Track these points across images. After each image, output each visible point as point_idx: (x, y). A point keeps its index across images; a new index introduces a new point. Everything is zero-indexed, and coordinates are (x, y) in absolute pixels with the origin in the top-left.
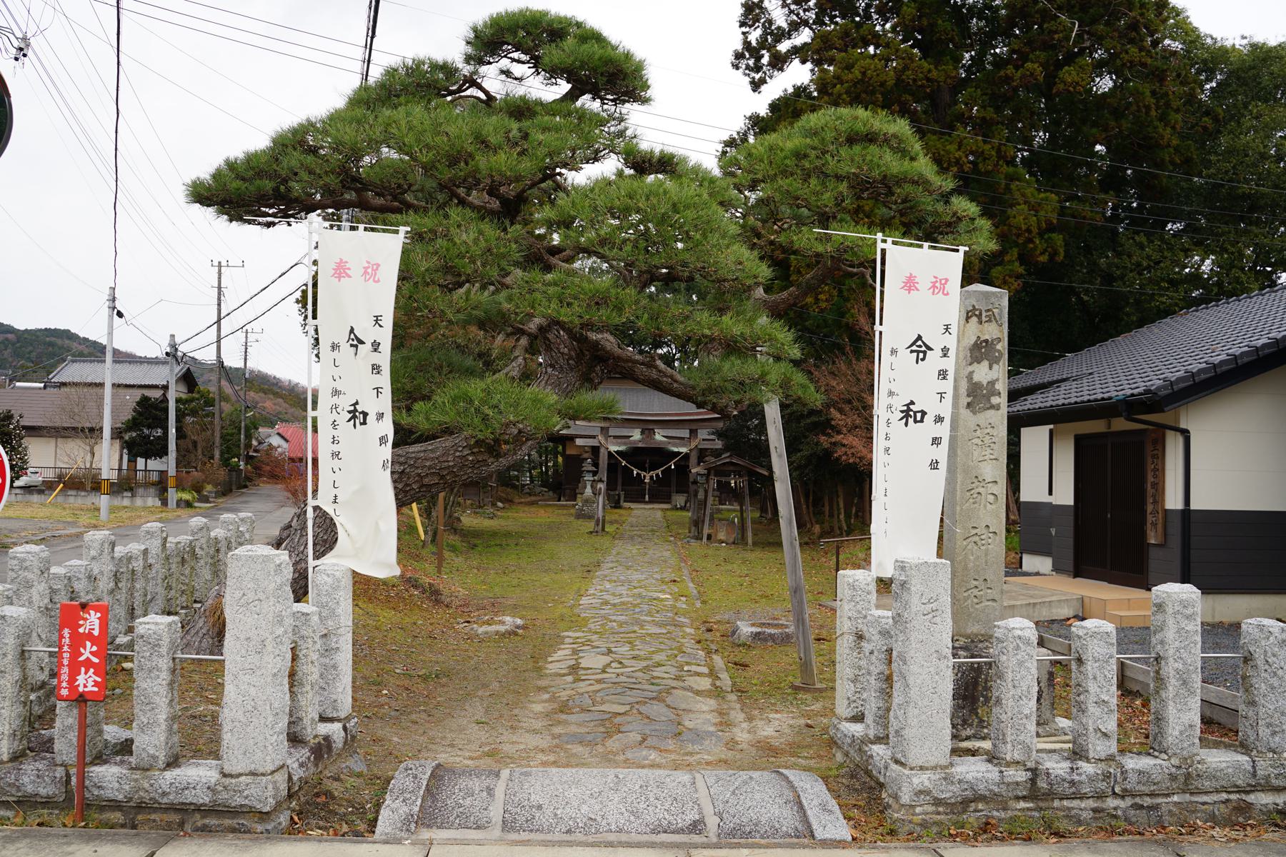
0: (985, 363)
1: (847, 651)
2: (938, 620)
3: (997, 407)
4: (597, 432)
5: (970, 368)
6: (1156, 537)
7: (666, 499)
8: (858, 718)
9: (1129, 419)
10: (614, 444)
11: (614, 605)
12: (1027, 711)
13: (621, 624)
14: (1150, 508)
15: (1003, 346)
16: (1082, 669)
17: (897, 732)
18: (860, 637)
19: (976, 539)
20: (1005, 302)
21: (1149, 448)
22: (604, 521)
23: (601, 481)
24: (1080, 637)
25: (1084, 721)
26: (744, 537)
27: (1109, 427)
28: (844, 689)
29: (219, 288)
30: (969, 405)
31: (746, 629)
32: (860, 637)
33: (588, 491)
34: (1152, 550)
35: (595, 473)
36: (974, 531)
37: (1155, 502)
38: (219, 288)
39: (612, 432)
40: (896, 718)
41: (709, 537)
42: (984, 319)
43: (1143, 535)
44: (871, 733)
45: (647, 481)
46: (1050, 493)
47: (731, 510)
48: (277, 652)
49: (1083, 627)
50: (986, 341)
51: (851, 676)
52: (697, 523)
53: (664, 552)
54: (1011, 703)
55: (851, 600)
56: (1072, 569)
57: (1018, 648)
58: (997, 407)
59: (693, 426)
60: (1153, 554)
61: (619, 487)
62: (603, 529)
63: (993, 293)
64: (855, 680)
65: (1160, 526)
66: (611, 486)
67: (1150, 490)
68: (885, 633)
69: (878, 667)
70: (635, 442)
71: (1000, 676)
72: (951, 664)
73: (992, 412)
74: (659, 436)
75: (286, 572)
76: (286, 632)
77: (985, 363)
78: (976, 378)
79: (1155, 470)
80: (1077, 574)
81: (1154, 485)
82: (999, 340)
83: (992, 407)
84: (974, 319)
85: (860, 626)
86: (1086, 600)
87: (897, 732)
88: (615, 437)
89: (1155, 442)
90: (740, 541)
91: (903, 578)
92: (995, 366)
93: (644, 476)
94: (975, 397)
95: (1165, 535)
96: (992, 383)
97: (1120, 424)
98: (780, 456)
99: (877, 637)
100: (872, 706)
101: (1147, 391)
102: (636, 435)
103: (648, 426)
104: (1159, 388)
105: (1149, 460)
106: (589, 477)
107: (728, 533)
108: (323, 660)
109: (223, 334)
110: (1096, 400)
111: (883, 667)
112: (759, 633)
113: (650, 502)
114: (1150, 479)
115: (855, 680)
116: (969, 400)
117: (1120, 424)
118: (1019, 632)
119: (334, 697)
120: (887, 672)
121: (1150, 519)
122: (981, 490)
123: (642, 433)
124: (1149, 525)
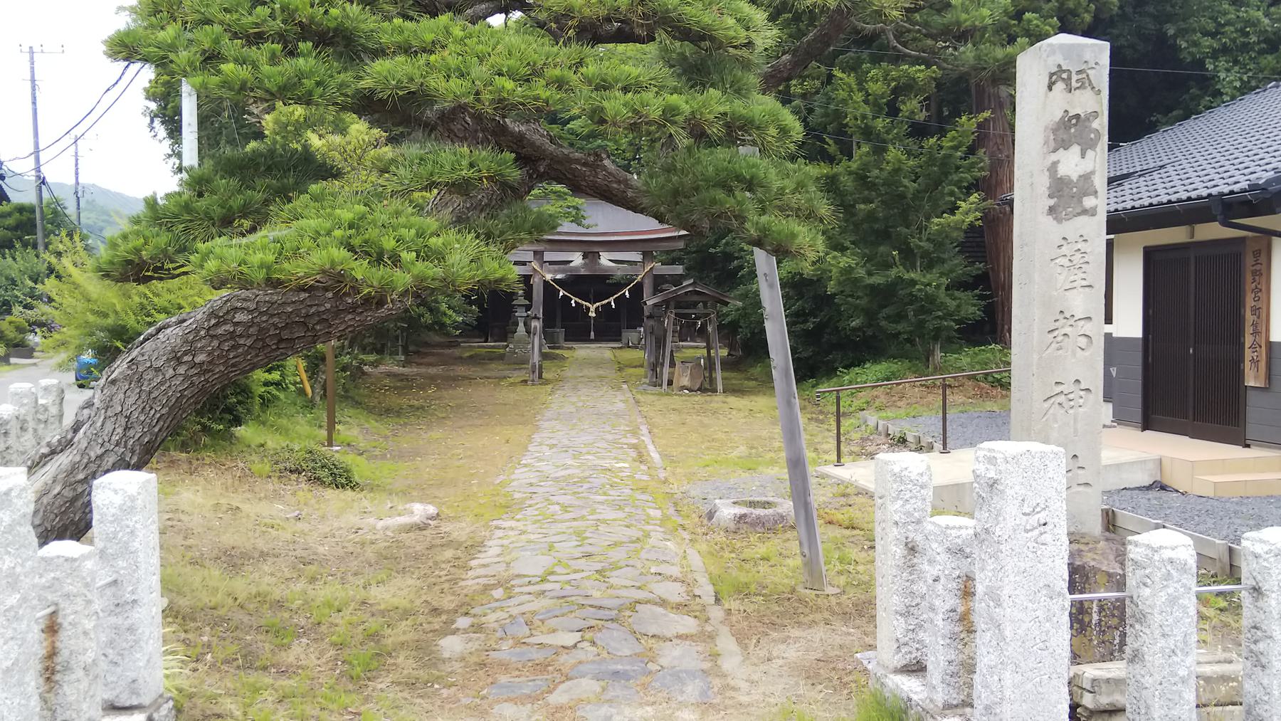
0: (1076, 149)
1: (894, 572)
2: (1047, 538)
3: (1092, 212)
4: (529, 256)
5: (1054, 157)
6: (1256, 378)
7: (616, 337)
8: (916, 668)
9: (1226, 224)
10: (550, 272)
11: (556, 479)
12: (1183, 672)
13: (565, 508)
14: (1248, 340)
15: (1102, 124)
16: (1260, 604)
17: (987, 708)
18: (912, 549)
19: (1061, 399)
20: (1105, 60)
21: (1249, 260)
22: (540, 367)
23: (536, 318)
24: (1257, 557)
25: (1265, 682)
26: (712, 380)
27: (1192, 236)
28: (889, 627)
29: (33, 80)
30: (1051, 210)
31: (727, 512)
32: (912, 549)
33: (521, 328)
34: (1250, 393)
35: (528, 308)
36: (1059, 389)
37: (1256, 333)
38: (33, 80)
39: (549, 256)
40: (986, 686)
41: (670, 383)
42: (1074, 84)
43: (1239, 374)
44: (940, 698)
45: (592, 314)
46: (1109, 320)
47: (694, 350)
48: (10, 633)
49: (1261, 541)
50: (1077, 116)
51: (901, 608)
52: (655, 367)
53: (617, 401)
54: (1159, 660)
55: (897, 498)
56: (1139, 417)
57: (1168, 576)
58: (1092, 212)
59: (647, 247)
60: (1253, 400)
61: (559, 323)
62: (540, 377)
63: (1086, 45)
64: (906, 614)
65: (1263, 364)
66: (549, 322)
67: (1249, 317)
68: (958, 552)
69: (945, 600)
70: (576, 268)
71: (1142, 618)
72: (1067, 604)
73: (1084, 218)
74: (605, 260)
75: (19, 503)
76: (24, 599)
77: (1076, 149)
78: (1062, 171)
79: (1257, 290)
80: (1146, 425)
81: (1256, 311)
82: (1095, 114)
83: (1085, 212)
84: (1060, 86)
85: (911, 535)
86: (1166, 463)
87: (987, 708)
88: (551, 263)
89: (1257, 254)
90: (707, 387)
91: (992, 474)
92: (1090, 153)
93: (590, 312)
94: (1059, 197)
95: (1269, 377)
96: (1086, 177)
97: (1212, 231)
98: (771, 286)
99: (943, 557)
100: (939, 658)
101: (1253, 187)
102: (577, 259)
103: (591, 250)
104: (1269, 182)
105: (1249, 278)
106: (520, 313)
107: (692, 377)
108: (113, 620)
109: (41, 147)
110: (1179, 201)
111: (952, 602)
112: (745, 516)
113: (596, 340)
114: (1249, 302)
115: (906, 614)
116: (1052, 202)
117: (1212, 231)
118: (1167, 554)
119: (132, 675)
120: (961, 609)
121: (1248, 354)
122: (1068, 330)
123: (585, 257)
124: (1247, 364)
